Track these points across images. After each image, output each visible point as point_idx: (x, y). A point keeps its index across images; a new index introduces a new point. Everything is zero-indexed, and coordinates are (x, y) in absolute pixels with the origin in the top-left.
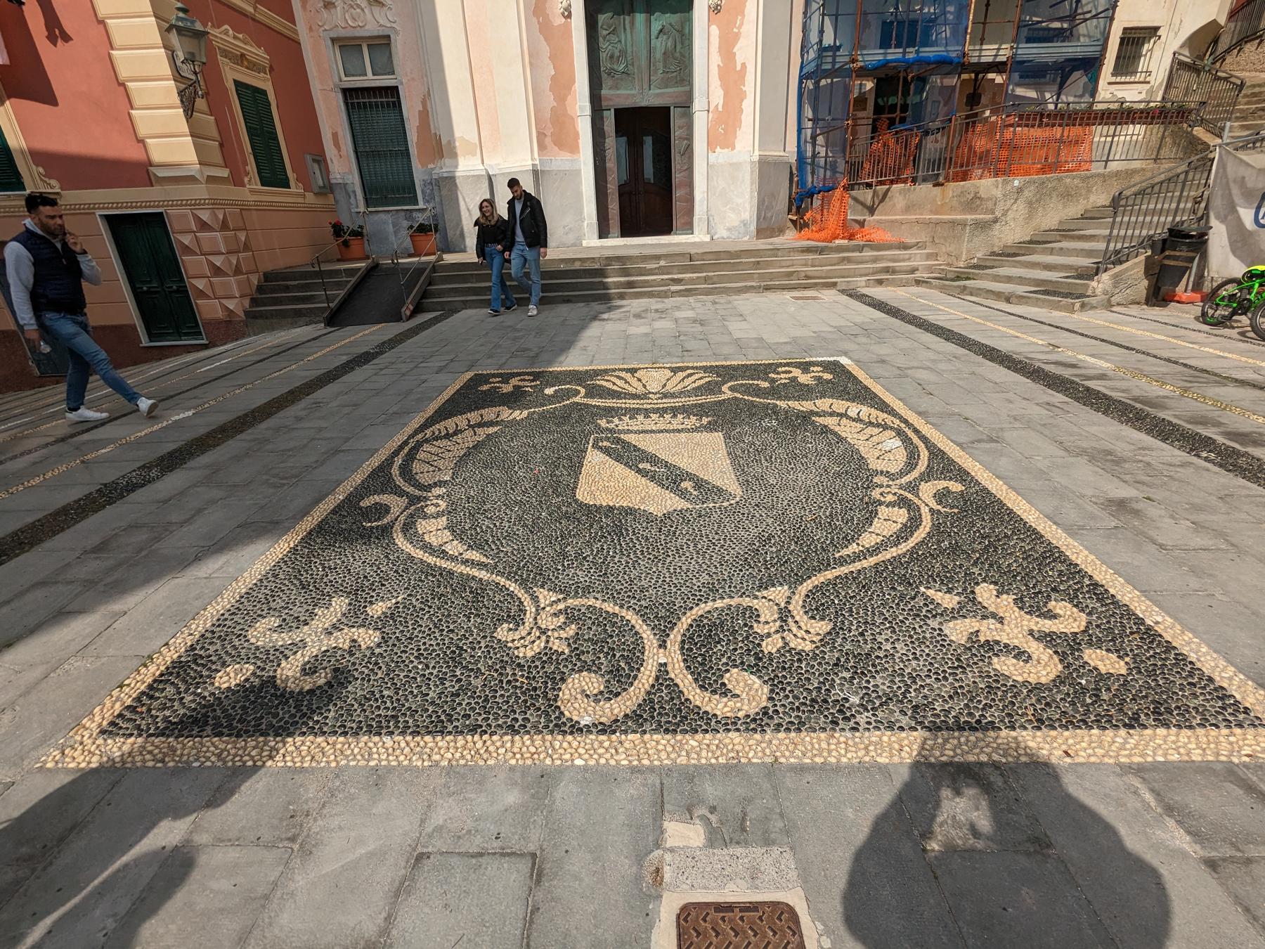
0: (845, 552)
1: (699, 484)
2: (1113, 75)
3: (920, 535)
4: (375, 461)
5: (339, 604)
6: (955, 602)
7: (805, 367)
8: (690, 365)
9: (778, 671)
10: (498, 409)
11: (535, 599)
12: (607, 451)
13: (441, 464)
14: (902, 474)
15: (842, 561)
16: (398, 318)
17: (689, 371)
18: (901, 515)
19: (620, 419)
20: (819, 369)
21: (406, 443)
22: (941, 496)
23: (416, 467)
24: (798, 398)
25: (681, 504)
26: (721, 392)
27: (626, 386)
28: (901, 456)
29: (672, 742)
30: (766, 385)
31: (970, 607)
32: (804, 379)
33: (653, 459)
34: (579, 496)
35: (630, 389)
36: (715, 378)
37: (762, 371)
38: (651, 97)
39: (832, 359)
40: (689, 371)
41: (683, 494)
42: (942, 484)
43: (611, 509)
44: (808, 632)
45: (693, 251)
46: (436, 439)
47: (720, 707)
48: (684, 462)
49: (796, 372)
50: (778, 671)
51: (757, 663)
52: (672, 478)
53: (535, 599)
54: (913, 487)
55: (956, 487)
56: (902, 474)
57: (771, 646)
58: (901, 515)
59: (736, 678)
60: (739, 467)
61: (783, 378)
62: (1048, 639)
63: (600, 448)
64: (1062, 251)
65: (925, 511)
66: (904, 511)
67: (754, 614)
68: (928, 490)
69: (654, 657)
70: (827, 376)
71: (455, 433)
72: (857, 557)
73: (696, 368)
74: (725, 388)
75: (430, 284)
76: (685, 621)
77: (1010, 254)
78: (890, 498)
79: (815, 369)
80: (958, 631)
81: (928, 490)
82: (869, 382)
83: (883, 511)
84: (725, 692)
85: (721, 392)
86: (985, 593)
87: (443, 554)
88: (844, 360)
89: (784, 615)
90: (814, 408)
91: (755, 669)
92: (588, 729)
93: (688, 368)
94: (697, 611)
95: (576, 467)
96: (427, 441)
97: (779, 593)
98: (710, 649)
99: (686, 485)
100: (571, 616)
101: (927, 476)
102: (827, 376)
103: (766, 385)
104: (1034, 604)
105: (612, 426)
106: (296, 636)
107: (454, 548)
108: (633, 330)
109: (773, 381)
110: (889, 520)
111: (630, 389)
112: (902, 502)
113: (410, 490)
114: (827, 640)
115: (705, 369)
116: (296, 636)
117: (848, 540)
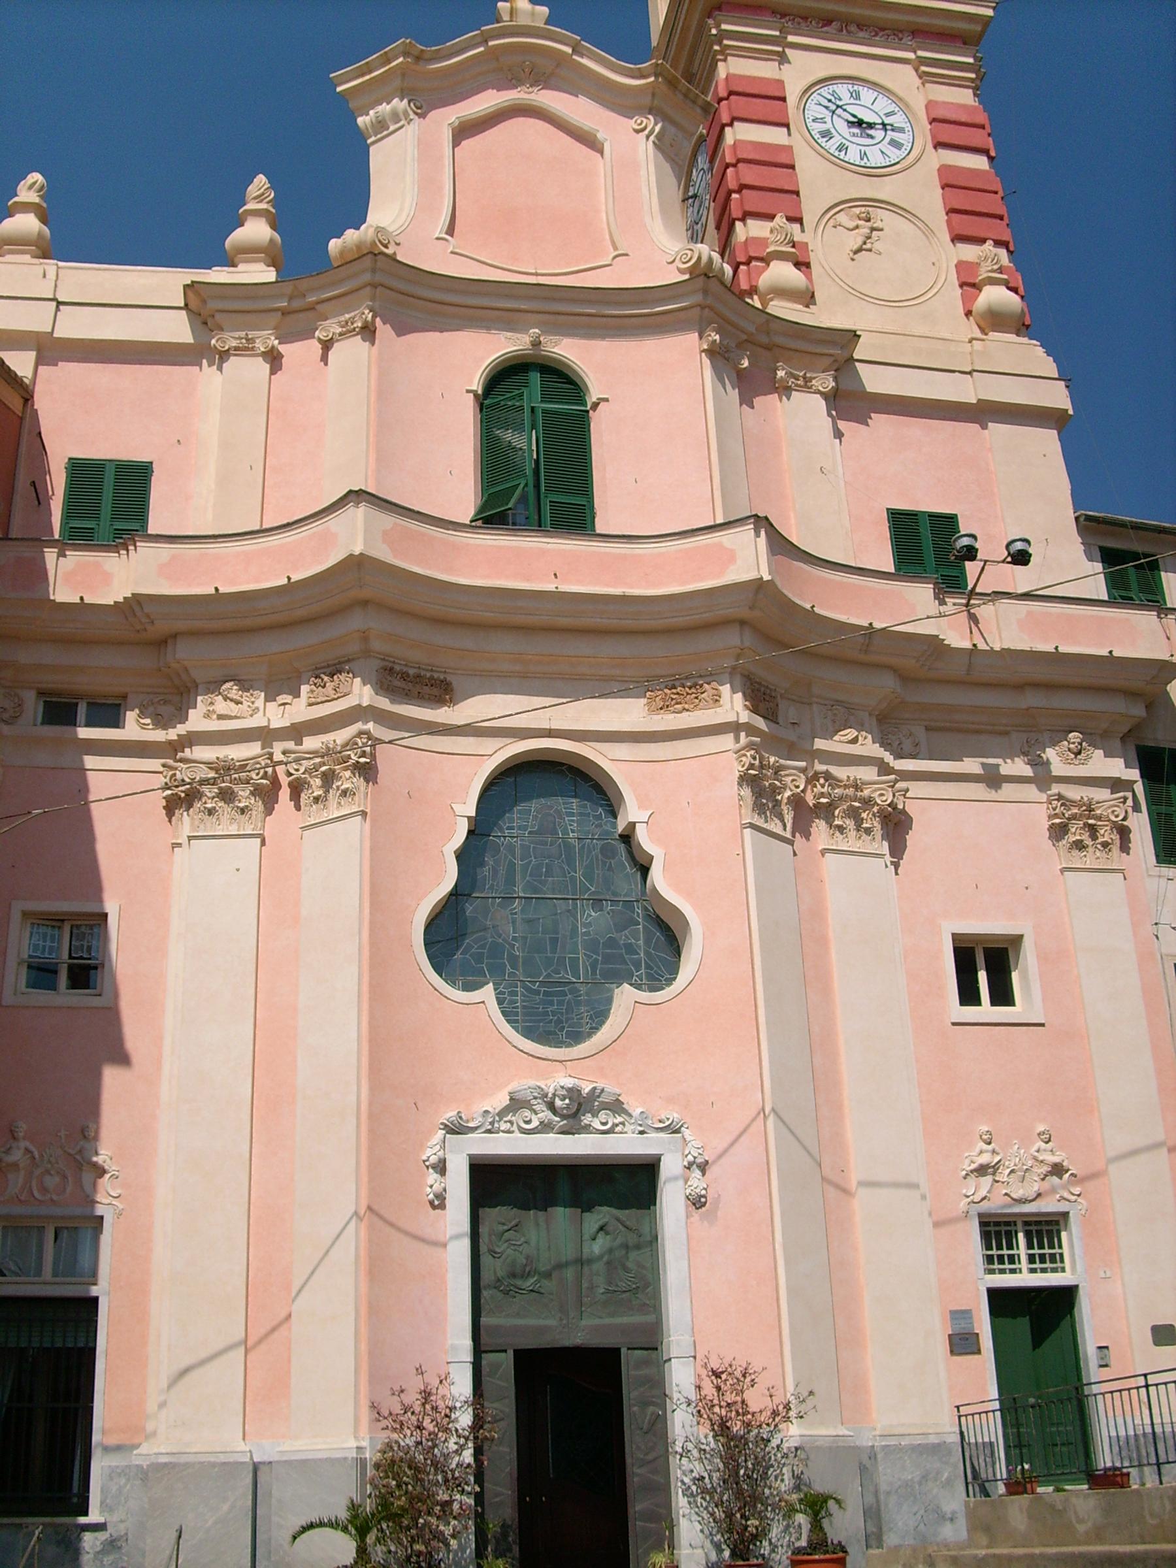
38: (583, 1331)
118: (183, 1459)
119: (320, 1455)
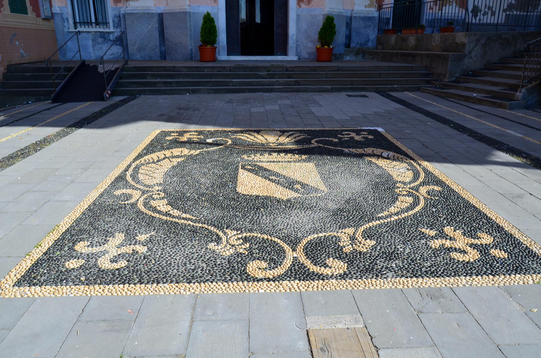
0: (380, 215)
1: (303, 185)
2: (27, 13)
3: (417, 209)
4: (117, 173)
5: (120, 237)
6: (434, 233)
7: (358, 132)
8: (291, 129)
9: (351, 259)
10: (383, 151)
11: (225, 233)
12: (249, 170)
13: (155, 175)
14: (410, 183)
15: (379, 219)
16: (102, 99)
17: (291, 133)
18: (410, 200)
19: (255, 156)
20: (366, 133)
21: (129, 166)
22: (428, 193)
23: (141, 177)
24: (352, 147)
25: (296, 195)
26: (311, 143)
27: (255, 139)
28: (410, 174)
29: (304, 283)
30: (336, 140)
31: (442, 235)
32: (357, 138)
33: (277, 175)
34: (239, 190)
35: (259, 141)
36: (306, 136)
37: (334, 133)
39: (373, 128)
40: (291, 133)
41: (297, 191)
42: (431, 187)
43: (257, 197)
44: (366, 245)
45: (288, 65)
46: (149, 163)
47: (327, 271)
48: (297, 176)
49: (353, 135)
50: (351, 259)
51: (340, 255)
52: (290, 184)
53: (225, 233)
54: (417, 189)
55: (436, 188)
56: (410, 183)
57: (348, 249)
58: (410, 200)
59: (330, 261)
60: (325, 179)
61: (346, 138)
62: (473, 246)
63: (245, 169)
64: (501, 76)
65: (421, 198)
66: (411, 198)
67: (338, 239)
68: (423, 190)
69: (290, 255)
70: (370, 137)
71: (158, 161)
72: (386, 217)
73: (295, 131)
74: (313, 141)
75: (120, 78)
76: (304, 242)
77: (475, 74)
78: (405, 193)
79: (364, 133)
80: (436, 244)
81: (423, 190)
82: (394, 141)
83: (401, 198)
84: (326, 266)
85: (311, 143)
86: (448, 230)
87: (170, 215)
88: (380, 129)
89: (353, 239)
90: (363, 152)
91: (340, 258)
92: (261, 280)
93: (291, 131)
94: (309, 238)
95: (234, 179)
96: (143, 164)
97: (350, 231)
98: (317, 251)
99: (298, 186)
100: (246, 240)
101: (423, 184)
102: (370, 137)
103: (336, 140)
104: (471, 233)
105: (250, 159)
106: (102, 248)
107: (176, 213)
108: (254, 110)
109: (340, 139)
110: (405, 201)
111: (259, 141)
112: (409, 194)
113: (142, 187)
114: (374, 248)
115: (301, 131)
116: (102, 248)
117: (382, 210)
118: (135, 12)
119: (177, 11)
